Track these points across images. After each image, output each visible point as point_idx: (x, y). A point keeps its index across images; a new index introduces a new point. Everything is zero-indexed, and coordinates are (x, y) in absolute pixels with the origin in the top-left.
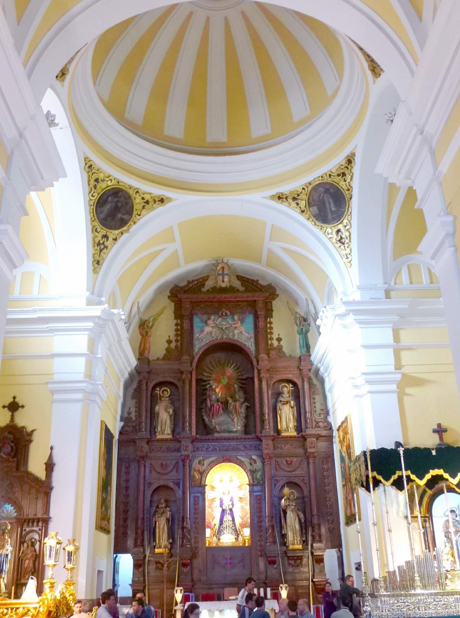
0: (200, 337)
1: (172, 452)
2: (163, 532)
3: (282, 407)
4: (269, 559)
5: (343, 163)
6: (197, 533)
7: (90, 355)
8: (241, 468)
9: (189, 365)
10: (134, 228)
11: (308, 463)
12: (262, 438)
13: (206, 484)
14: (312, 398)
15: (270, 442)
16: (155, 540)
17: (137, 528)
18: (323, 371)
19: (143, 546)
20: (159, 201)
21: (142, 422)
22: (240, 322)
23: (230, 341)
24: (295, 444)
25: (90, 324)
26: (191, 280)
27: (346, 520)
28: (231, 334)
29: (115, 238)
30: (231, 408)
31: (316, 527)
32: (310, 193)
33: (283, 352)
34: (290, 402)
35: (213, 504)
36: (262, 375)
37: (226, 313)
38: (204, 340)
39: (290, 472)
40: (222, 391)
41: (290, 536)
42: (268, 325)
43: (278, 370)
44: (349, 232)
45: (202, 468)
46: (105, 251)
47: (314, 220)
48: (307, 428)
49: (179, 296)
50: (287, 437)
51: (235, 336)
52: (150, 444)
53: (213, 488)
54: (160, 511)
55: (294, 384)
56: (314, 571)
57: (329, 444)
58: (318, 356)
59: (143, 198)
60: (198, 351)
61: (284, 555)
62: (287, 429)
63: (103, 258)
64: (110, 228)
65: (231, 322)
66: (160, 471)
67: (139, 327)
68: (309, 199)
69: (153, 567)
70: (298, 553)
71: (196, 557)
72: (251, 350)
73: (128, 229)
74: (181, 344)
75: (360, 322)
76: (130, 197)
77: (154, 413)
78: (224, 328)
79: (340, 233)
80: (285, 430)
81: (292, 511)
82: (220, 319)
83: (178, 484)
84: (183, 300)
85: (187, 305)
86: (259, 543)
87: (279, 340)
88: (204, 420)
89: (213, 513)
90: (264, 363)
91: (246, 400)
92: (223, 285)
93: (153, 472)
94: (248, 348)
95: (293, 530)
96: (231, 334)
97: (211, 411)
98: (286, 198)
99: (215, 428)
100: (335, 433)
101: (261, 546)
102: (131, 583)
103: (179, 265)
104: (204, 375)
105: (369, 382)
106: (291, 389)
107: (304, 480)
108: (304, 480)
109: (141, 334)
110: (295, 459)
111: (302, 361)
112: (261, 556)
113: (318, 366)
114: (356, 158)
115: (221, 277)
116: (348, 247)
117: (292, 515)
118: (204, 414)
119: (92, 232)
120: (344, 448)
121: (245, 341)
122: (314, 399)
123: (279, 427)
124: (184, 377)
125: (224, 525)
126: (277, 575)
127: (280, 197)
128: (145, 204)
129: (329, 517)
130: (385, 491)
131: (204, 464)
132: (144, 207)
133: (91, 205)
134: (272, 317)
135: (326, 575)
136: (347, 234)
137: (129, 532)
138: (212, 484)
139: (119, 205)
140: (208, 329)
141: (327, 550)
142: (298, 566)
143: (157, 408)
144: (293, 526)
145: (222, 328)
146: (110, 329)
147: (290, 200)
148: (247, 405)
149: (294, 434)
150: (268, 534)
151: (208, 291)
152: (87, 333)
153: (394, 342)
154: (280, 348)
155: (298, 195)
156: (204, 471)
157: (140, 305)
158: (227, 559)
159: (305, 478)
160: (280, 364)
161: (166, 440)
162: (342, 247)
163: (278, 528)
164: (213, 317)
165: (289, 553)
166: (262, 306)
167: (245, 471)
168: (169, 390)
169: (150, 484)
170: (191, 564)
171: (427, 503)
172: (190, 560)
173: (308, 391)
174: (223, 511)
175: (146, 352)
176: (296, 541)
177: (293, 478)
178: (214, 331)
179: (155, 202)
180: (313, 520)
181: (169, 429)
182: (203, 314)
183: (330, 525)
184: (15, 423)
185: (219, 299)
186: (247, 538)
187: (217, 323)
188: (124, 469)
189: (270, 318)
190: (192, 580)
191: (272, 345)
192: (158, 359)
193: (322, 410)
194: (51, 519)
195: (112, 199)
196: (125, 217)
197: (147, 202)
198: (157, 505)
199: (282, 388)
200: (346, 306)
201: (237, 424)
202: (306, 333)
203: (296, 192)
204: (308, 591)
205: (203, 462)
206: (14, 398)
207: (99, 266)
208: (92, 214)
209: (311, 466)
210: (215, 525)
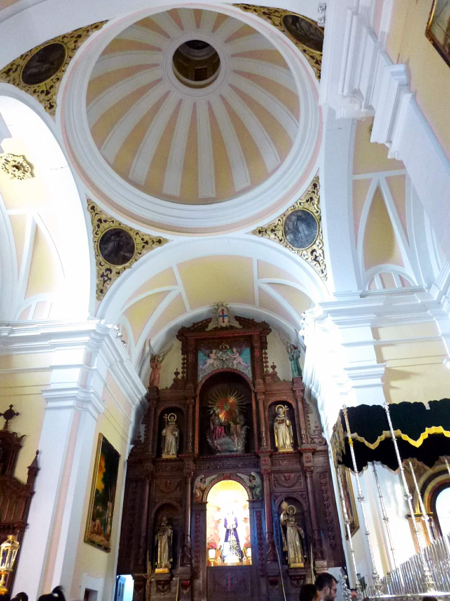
0: (203, 368)
4: (270, 579)
5: (310, 189)
7: (85, 366)
9: (193, 391)
10: (135, 264)
11: (306, 478)
12: (260, 455)
13: (207, 501)
14: (306, 417)
15: (268, 459)
20: (157, 242)
23: (230, 370)
24: (293, 460)
25: (87, 338)
26: (196, 322)
29: (118, 272)
30: (232, 430)
31: (317, 543)
32: (285, 223)
33: (278, 377)
34: (286, 421)
36: (258, 397)
37: (225, 347)
39: (288, 487)
42: (264, 356)
43: (274, 393)
44: (322, 250)
45: (203, 486)
46: (108, 282)
47: (291, 246)
48: (302, 443)
50: (284, 453)
55: (289, 405)
57: (325, 459)
58: (308, 376)
59: (143, 239)
60: (202, 381)
63: (106, 287)
64: (114, 263)
65: (230, 354)
68: (285, 229)
72: (249, 377)
73: (131, 265)
74: (187, 376)
75: (339, 323)
76: (131, 238)
78: (224, 359)
79: (314, 253)
80: (282, 447)
81: (292, 527)
82: (221, 353)
87: (274, 367)
90: (260, 387)
92: (224, 325)
94: (246, 375)
97: (213, 434)
98: (266, 231)
99: (217, 448)
103: (185, 311)
105: (353, 378)
106: (286, 409)
107: (302, 495)
110: (293, 475)
112: (263, 576)
114: (320, 181)
115: (221, 318)
116: (322, 263)
119: (97, 265)
121: (243, 369)
122: (308, 417)
123: (277, 445)
124: (188, 401)
127: (261, 232)
128: (145, 244)
130: (375, 471)
131: (205, 482)
132: (143, 247)
133: (95, 242)
134: (267, 349)
136: (321, 251)
139: (121, 243)
140: (210, 361)
144: (293, 543)
145: (222, 360)
146: (106, 342)
147: (269, 232)
149: (291, 450)
151: (211, 331)
152: (84, 346)
153: (374, 338)
154: (274, 375)
155: (276, 227)
156: (206, 488)
160: (275, 387)
162: (318, 265)
163: (279, 546)
164: (214, 351)
167: (245, 488)
171: (428, 499)
174: (228, 531)
175: (156, 382)
176: (297, 559)
179: (153, 242)
181: (174, 450)
182: (206, 349)
183: (332, 541)
184: (8, 429)
187: (219, 355)
191: (267, 371)
192: (167, 388)
193: (316, 427)
194: (29, 526)
195: (114, 238)
196: (127, 255)
197: (147, 243)
199: (278, 408)
201: (238, 444)
203: (273, 224)
206: (11, 406)
208: (96, 250)
209: (309, 480)
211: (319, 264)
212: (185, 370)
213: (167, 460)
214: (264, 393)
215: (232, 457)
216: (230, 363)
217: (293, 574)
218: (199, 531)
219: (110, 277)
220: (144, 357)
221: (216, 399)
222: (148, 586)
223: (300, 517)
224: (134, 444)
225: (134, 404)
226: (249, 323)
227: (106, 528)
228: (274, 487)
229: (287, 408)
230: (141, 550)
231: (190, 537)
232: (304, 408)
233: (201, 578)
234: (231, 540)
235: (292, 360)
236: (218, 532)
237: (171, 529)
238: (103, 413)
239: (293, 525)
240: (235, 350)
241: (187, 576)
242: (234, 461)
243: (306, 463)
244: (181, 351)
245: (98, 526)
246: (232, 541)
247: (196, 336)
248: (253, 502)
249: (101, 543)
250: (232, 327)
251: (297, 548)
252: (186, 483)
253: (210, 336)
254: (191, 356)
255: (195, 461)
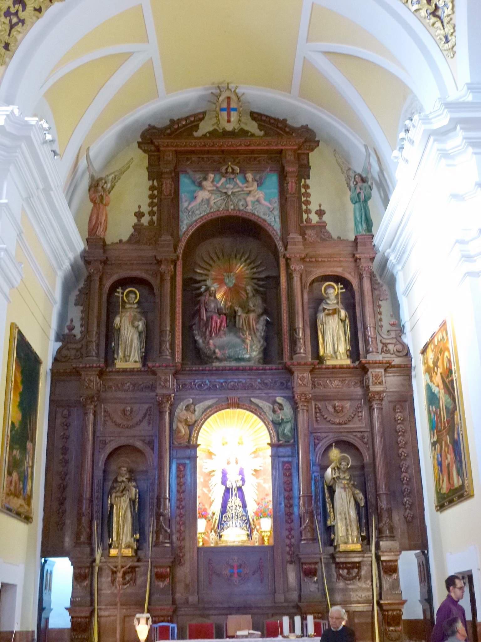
1: (142, 390)
2: (124, 522)
3: (325, 319)
4: (304, 567)
6: (183, 524)
8: (259, 420)
9: (172, 249)
11: (371, 409)
12: (293, 368)
13: (198, 443)
14: (376, 306)
15: (306, 375)
16: (110, 535)
17: (80, 515)
18: (394, 261)
19: (90, 542)
21: (91, 342)
22: (256, 184)
23: (238, 214)
24: (349, 379)
26: (176, 119)
27: (439, 501)
28: (241, 203)
29: (38, 7)
33: (328, 232)
34: (339, 311)
35: (210, 480)
36: (293, 267)
37: (233, 169)
38: (197, 212)
39: (340, 424)
40: (228, 297)
41: (341, 530)
42: (303, 190)
45: (191, 418)
46: (19, 27)
48: (367, 352)
49: (156, 142)
50: (334, 367)
51: (247, 206)
52: (105, 377)
53: (210, 455)
54: (120, 487)
56: (381, 587)
57: (404, 380)
60: (187, 230)
61: (331, 561)
62: (334, 355)
63: (16, 40)
65: (240, 184)
66: (119, 421)
67: (89, 190)
69: (106, 579)
70: (355, 557)
71: (180, 563)
74: (159, 219)
77: (113, 327)
78: (230, 193)
80: (332, 357)
81: (344, 488)
82: (223, 180)
83: (150, 444)
84: (162, 149)
85: (170, 157)
86: (288, 541)
87: (320, 213)
88: (195, 342)
89: (210, 495)
91: (265, 312)
93: (109, 423)
94: (270, 225)
95: (346, 519)
96: (241, 203)
97: (207, 328)
99: (214, 352)
100: (418, 362)
101: (290, 546)
102: (68, 605)
104: (196, 272)
106: (340, 291)
107: (362, 438)
108: (362, 438)
109: (92, 200)
110: (348, 404)
111: (359, 245)
112: (291, 562)
113: (386, 254)
115: (225, 114)
116: (448, 23)
117: (344, 494)
118: (196, 332)
120: (438, 379)
121: (264, 215)
122: (379, 306)
123: (321, 352)
124: (163, 268)
125: (229, 514)
126: (319, 595)
129: (405, 499)
131: (195, 411)
135: (401, 594)
137: (68, 522)
138: (209, 448)
140: (202, 195)
141: (404, 553)
142: (354, 578)
143: (117, 320)
144: (345, 514)
145: (226, 193)
146: (23, 153)
148: (267, 321)
149: (347, 362)
150: (303, 527)
151: (204, 136)
154: (322, 226)
156: (195, 422)
157: (91, 154)
158: (232, 567)
159: (366, 435)
160: (323, 250)
161: (131, 372)
162: (439, 24)
163: (320, 517)
164: (211, 176)
165: (339, 557)
166: (292, 158)
167: (265, 423)
168: (137, 292)
169: (105, 443)
170: (172, 575)
172: (170, 567)
173: (370, 294)
174: (228, 491)
176: (350, 538)
177: (343, 434)
178: (213, 198)
180: (379, 502)
183: (408, 511)
185: (221, 146)
186: (266, 534)
187: (219, 185)
188: (59, 420)
189: (305, 179)
190: (174, 602)
191: (308, 220)
192: (121, 241)
198: (113, 478)
200: (450, 112)
201: (251, 347)
202: (366, 201)
204: (370, 620)
205: (193, 407)
207: (8, 52)
209: (376, 414)
210: (214, 514)
211: (442, 22)
212: (155, 209)
213: (124, 371)
214: (303, 260)
215: (244, 369)
216: (240, 200)
217: (342, 560)
218: (183, 492)
219: (22, 18)
220: (75, 180)
221: (210, 265)
222: (119, 581)
223: (357, 473)
224: (62, 341)
225: (60, 269)
226: (278, 127)
227: (26, 486)
228: (315, 423)
229: (342, 289)
230: (84, 518)
231: (169, 500)
232: (373, 289)
233: (187, 565)
234: (233, 504)
235: (356, 202)
236: (210, 491)
237: (134, 487)
238: (17, 288)
239: (346, 486)
240: (250, 176)
241: (167, 561)
242: (247, 377)
243: (373, 385)
244: (146, 173)
245: (16, 484)
246: (234, 506)
247: (177, 146)
248: (279, 446)
249: (21, 510)
250: (243, 133)
251: (351, 522)
252: (161, 413)
253: (195, 146)
254: (167, 185)
255: (176, 374)
